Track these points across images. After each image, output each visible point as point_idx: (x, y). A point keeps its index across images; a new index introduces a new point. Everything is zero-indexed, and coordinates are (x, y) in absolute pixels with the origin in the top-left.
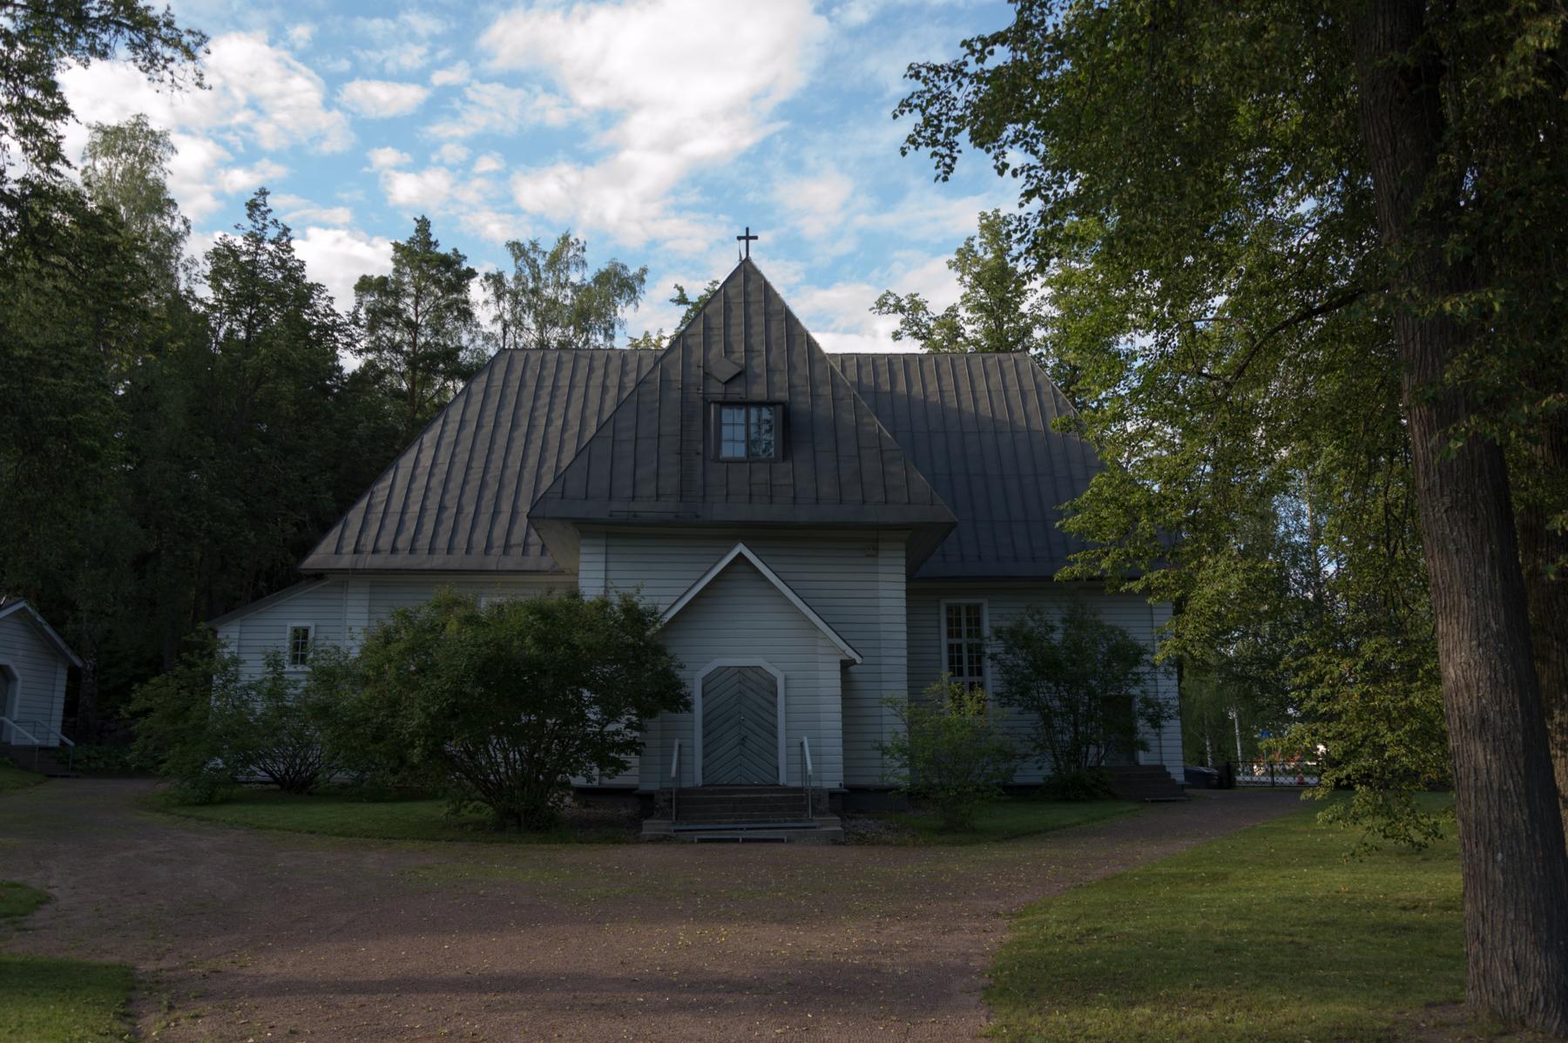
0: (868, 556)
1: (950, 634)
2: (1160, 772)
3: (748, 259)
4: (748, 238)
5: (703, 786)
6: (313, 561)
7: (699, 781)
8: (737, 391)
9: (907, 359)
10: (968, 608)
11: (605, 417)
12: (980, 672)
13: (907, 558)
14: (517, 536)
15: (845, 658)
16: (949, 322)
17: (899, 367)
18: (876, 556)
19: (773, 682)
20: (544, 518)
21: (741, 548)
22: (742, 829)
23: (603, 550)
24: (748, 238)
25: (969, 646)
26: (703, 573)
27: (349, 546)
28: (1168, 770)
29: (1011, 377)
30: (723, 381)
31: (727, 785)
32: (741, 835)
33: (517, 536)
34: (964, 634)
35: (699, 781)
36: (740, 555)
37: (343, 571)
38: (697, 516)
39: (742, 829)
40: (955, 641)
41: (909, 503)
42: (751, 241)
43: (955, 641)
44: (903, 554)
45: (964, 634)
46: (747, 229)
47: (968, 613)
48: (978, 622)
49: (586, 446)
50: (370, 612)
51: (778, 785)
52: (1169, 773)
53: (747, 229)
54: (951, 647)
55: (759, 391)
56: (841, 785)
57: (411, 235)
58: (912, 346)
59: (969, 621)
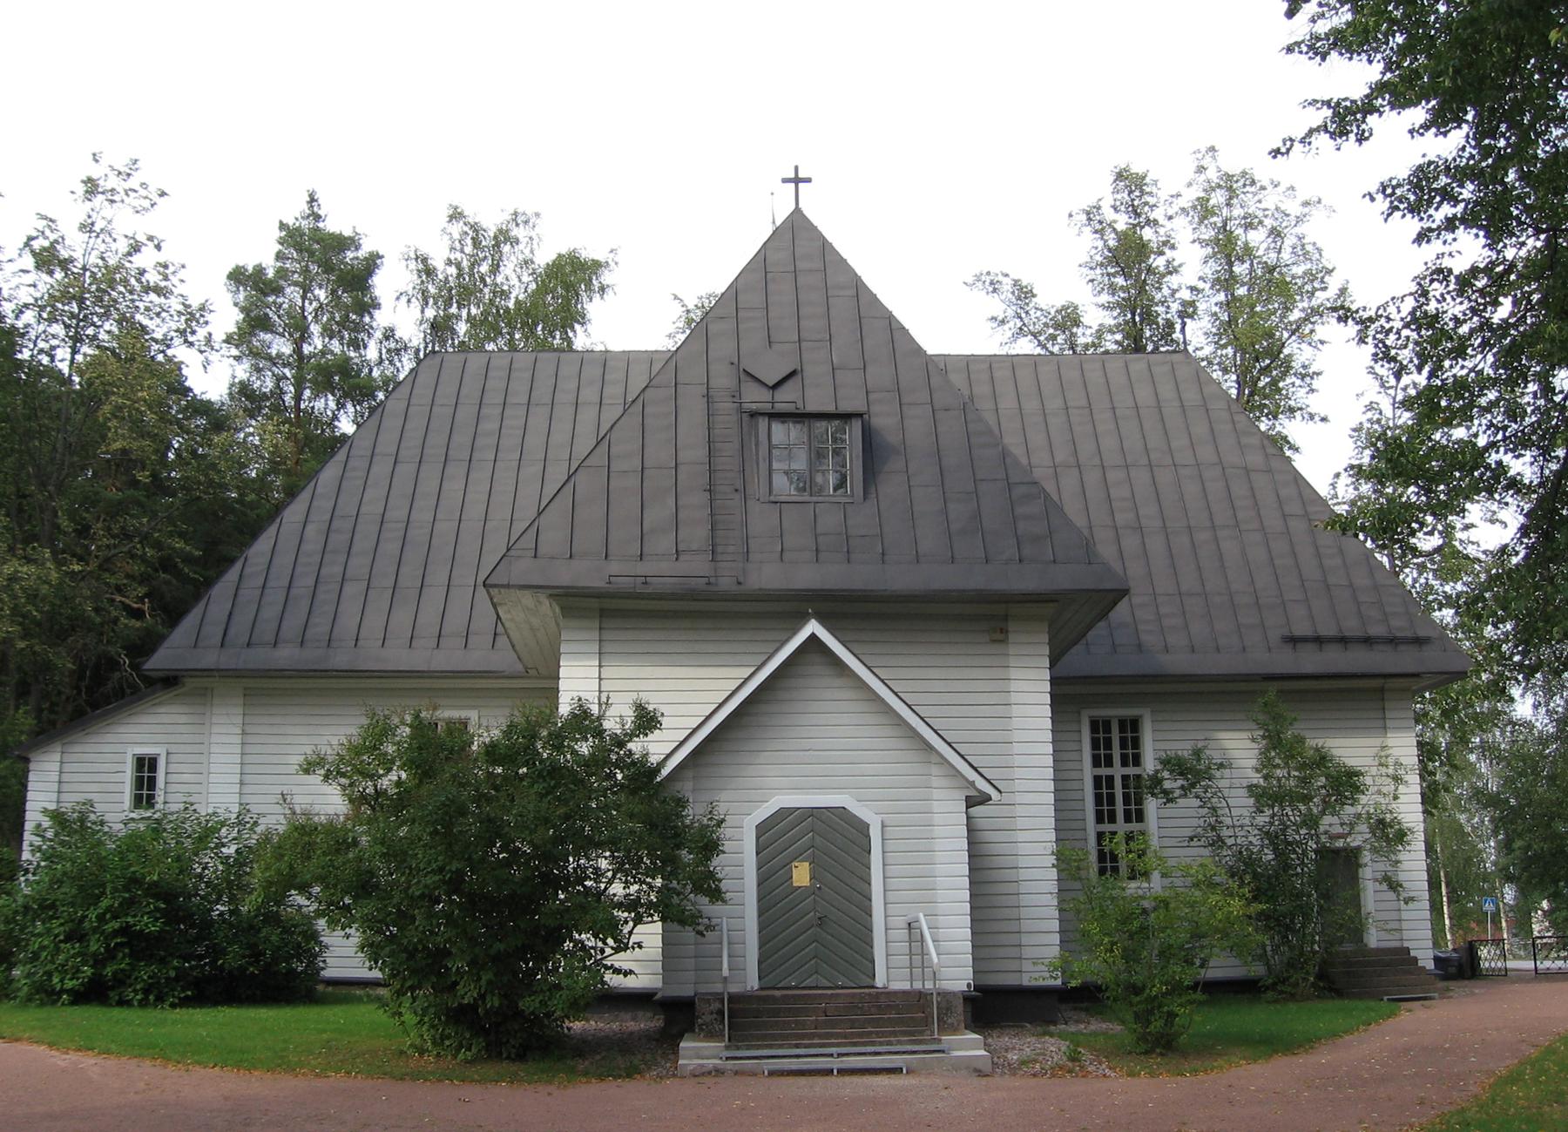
0: (994, 641)
1: (1096, 762)
2: (1401, 959)
3: (797, 211)
4: (797, 180)
5: (761, 989)
6: (158, 661)
7: (753, 983)
8: (787, 398)
9: (1013, 361)
10: (1122, 724)
11: (519, 527)
12: (1140, 817)
13: (1050, 643)
14: (457, 620)
15: (973, 793)
16: (1068, 319)
17: (1001, 374)
18: (1004, 641)
19: (863, 828)
20: (508, 586)
21: (813, 627)
22: (832, 1055)
23: (596, 635)
24: (797, 180)
25: (1125, 778)
26: (764, 657)
27: (213, 631)
28: (1413, 953)
29: (1167, 391)
30: (771, 385)
31: (796, 988)
32: (835, 1063)
33: (457, 620)
34: (1117, 759)
35: (753, 983)
36: (813, 637)
37: (207, 672)
38: (739, 583)
39: (832, 1055)
40: (1104, 771)
41: (1054, 561)
42: (801, 185)
43: (1104, 771)
44: (1047, 637)
45: (1117, 759)
46: (796, 168)
47: (1122, 729)
48: (1136, 743)
49: (606, 435)
50: (244, 733)
51: (873, 987)
52: (1416, 959)
53: (796, 168)
54: (1097, 780)
55: (817, 401)
56: (969, 985)
57: (276, 250)
58: (1026, 346)
59: (1123, 745)
